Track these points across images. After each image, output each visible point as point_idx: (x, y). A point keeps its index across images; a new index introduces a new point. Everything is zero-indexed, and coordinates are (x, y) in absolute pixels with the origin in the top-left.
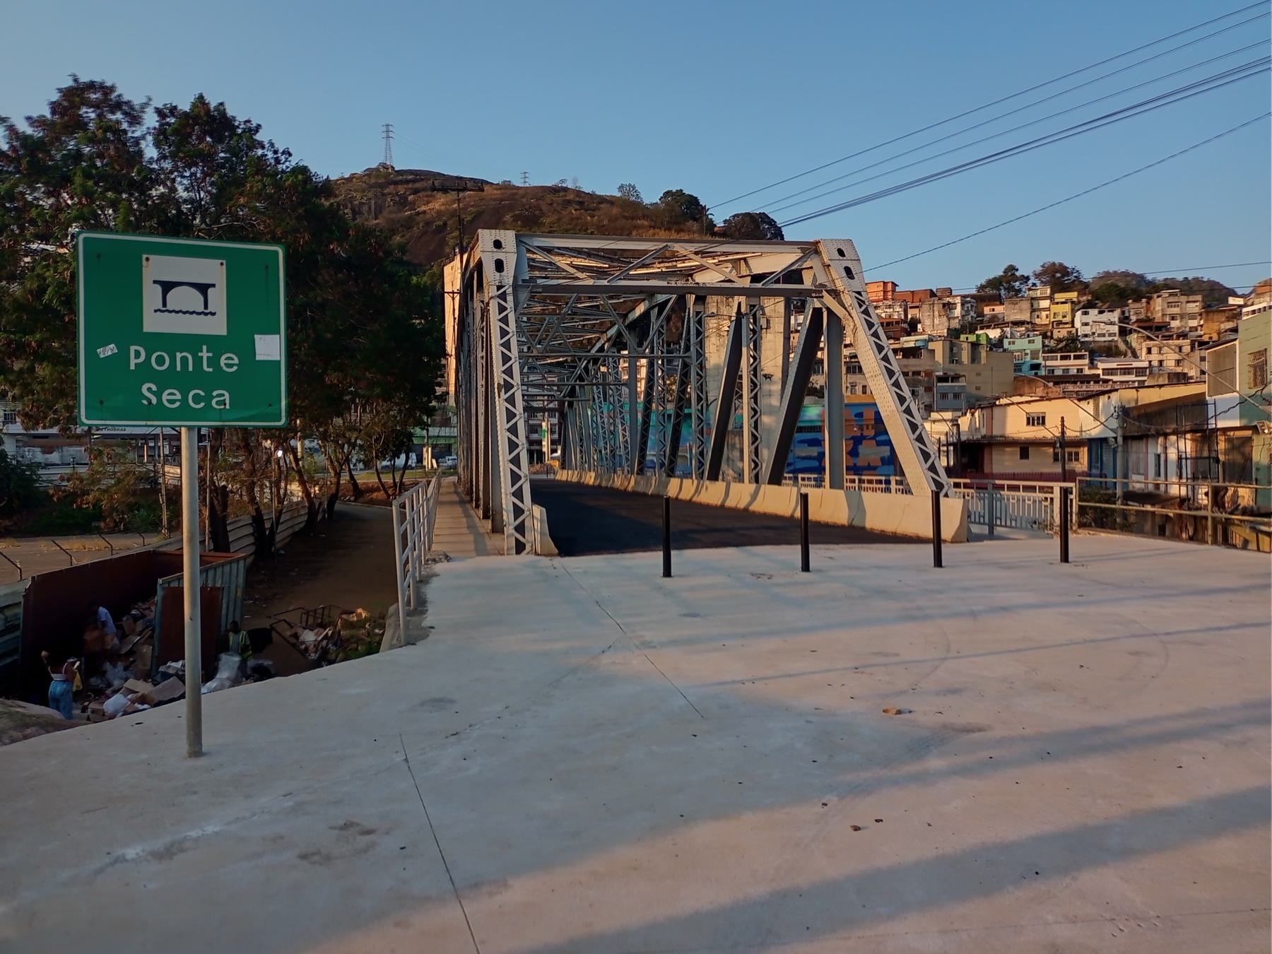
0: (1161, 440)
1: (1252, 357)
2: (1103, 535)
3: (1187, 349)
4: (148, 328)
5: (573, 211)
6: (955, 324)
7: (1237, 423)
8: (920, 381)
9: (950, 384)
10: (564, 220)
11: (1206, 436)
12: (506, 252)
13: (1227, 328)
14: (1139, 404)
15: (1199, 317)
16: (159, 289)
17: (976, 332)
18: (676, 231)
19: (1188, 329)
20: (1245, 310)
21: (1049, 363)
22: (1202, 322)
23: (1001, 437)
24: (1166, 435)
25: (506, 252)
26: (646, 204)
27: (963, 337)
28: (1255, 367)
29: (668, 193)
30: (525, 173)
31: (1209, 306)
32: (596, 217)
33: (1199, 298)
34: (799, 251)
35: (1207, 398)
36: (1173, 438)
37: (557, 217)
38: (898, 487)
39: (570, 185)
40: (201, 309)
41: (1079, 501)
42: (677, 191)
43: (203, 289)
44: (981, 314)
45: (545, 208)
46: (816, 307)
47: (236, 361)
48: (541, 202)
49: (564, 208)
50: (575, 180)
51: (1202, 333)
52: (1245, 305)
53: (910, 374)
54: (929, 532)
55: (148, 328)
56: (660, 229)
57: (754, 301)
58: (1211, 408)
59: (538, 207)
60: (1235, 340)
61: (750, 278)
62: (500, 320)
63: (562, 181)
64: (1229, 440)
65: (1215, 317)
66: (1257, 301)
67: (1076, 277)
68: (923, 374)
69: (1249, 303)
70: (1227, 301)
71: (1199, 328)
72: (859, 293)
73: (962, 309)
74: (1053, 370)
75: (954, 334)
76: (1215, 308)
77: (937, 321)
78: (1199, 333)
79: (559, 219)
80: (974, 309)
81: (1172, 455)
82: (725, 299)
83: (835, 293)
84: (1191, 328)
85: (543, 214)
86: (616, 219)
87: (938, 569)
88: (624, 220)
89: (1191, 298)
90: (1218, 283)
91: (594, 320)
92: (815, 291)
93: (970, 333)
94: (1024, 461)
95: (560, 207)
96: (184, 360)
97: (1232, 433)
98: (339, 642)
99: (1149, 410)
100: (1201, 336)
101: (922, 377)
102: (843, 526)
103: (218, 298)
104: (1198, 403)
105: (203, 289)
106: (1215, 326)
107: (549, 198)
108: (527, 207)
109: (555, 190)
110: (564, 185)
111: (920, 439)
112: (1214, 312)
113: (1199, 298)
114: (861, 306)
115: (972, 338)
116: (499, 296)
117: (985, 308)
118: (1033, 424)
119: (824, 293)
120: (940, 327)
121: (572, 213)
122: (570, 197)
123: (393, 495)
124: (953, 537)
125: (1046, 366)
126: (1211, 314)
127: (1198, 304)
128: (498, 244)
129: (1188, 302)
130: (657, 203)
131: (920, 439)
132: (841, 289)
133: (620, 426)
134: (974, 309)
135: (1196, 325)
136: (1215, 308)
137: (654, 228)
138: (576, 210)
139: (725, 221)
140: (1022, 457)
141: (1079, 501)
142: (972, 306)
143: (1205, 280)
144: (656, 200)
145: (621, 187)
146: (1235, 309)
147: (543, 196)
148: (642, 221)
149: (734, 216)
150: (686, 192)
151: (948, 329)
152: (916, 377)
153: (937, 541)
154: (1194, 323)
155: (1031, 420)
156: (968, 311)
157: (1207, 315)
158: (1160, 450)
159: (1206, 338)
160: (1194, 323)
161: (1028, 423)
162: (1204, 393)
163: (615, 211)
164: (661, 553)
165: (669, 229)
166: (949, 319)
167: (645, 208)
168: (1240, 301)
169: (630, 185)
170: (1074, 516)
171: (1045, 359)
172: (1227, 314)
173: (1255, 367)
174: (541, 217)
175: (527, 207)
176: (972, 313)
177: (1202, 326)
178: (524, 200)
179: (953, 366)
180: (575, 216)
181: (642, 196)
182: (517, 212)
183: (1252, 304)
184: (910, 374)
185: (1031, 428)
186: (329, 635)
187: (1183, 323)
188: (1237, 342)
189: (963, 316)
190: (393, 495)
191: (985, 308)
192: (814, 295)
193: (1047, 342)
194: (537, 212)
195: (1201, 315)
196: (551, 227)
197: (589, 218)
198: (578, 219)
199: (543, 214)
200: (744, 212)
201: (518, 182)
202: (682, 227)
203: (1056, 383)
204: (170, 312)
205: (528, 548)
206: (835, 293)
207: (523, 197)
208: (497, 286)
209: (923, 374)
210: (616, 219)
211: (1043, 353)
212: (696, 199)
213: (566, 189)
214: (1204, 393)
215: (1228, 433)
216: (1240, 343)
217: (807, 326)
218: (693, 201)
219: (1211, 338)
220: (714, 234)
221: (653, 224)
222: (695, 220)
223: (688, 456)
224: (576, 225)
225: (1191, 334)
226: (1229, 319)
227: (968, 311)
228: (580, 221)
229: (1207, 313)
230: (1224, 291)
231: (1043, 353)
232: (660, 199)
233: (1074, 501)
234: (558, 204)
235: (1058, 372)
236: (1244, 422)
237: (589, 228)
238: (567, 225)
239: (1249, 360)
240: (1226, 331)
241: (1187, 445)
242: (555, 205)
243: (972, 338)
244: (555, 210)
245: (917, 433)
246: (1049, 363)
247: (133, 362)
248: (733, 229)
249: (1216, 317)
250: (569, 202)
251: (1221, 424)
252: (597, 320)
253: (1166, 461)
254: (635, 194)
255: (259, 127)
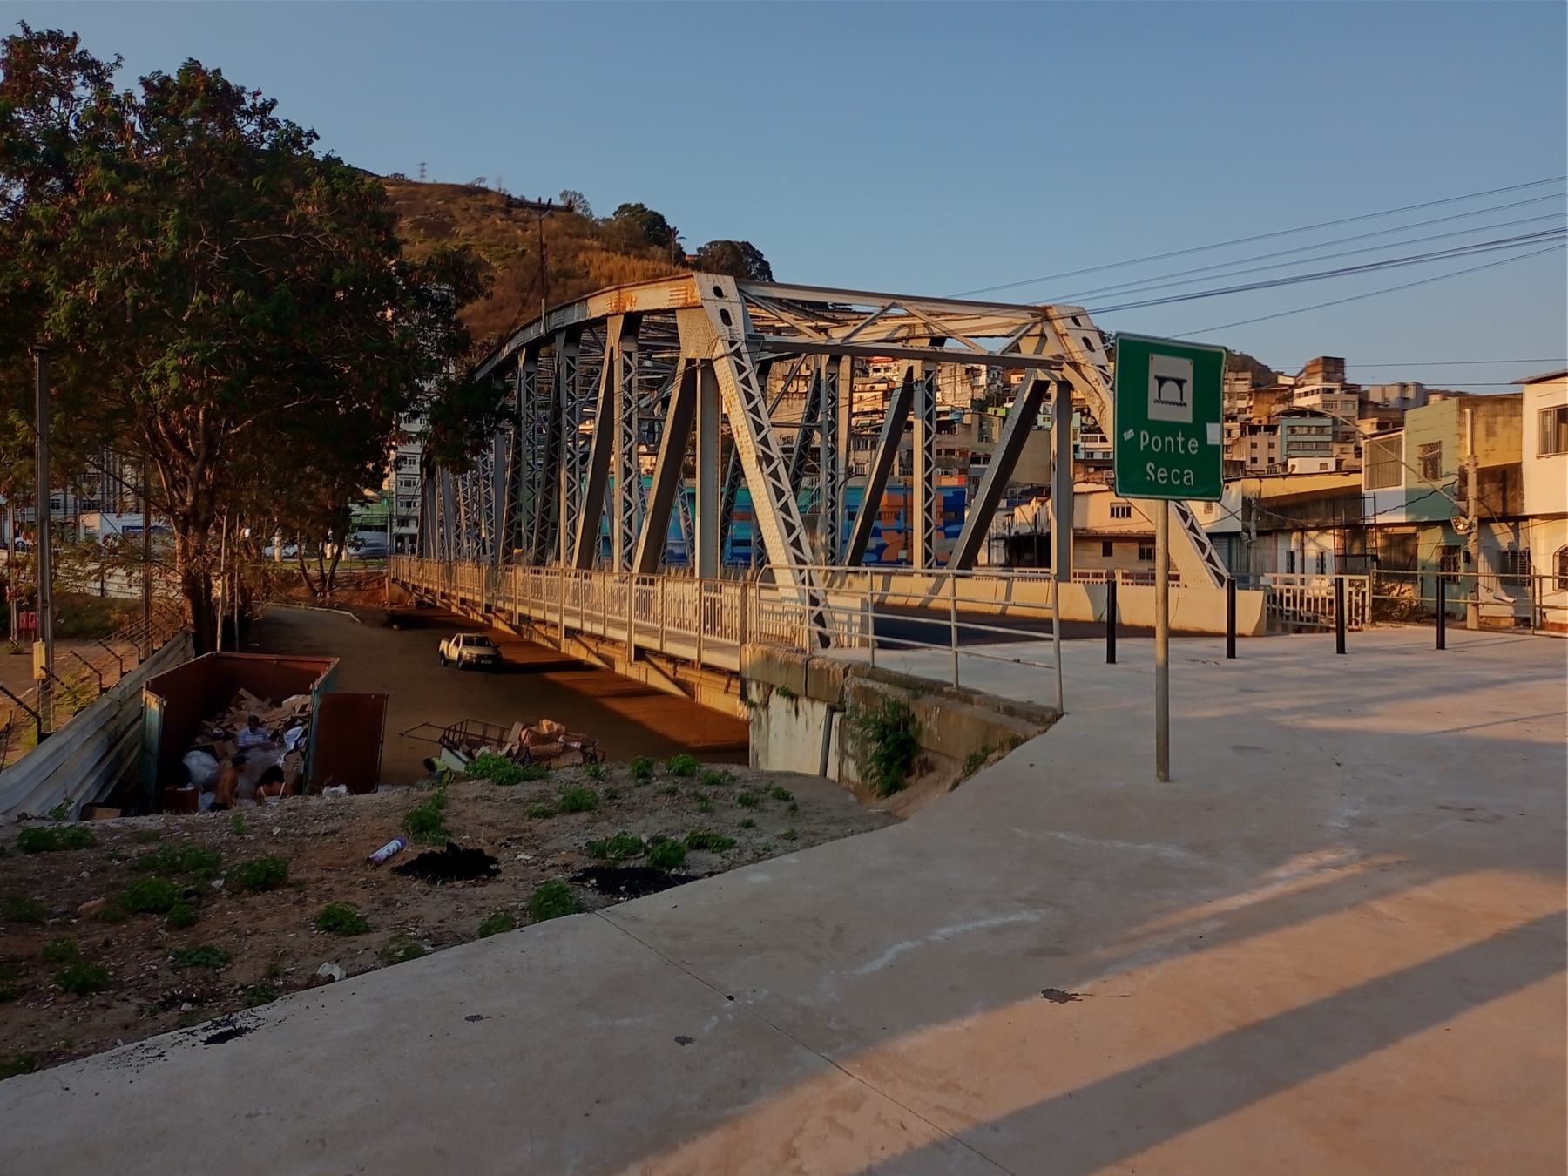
0: (1295, 535)
1: (1421, 449)
2: (1408, 627)
3: (1236, 433)
4: (1152, 415)
5: (498, 221)
6: (980, 394)
7: (1402, 519)
8: (954, 461)
9: (981, 466)
10: (484, 232)
11: (1356, 530)
12: (730, 302)
13: (1278, 411)
14: (1263, 496)
15: (1248, 398)
16: (1157, 382)
17: (1005, 405)
18: (635, 257)
19: (1236, 411)
20: (1297, 391)
21: (1089, 445)
22: (1251, 403)
23: (1083, 530)
24: (1303, 530)
25: (730, 302)
26: (597, 219)
27: (991, 410)
28: (1425, 460)
29: (624, 208)
30: (423, 164)
31: (1259, 385)
32: (529, 232)
33: (1248, 375)
34: (1029, 316)
35: (1364, 491)
36: (1313, 534)
37: (475, 227)
38: (1125, 581)
39: (491, 185)
40: (1178, 400)
41: (1374, 594)
42: (637, 205)
43: (1180, 383)
44: (1008, 384)
45: (457, 214)
46: (1040, 378)
47: (1197, 445)
48: (452, 206)
49: (485, 216)
50: (499, 180)
51: (1251, 415)
52: (1296, 386)
53: (943, 452)
54: (1224, 628)
55: (1152, 415)
56: (616, 253)
57: (930, 367)
58: (1369, 504)
59: (449, 213)
60: (1401, 430)
61: (929, 340)
62: (741, 382)
63: (481, 179)
64: (1388, 537)
65: (1265, 398)
66: (1308, 382)
67: (1112, 344)
68: (957, 453)
69: (1300, 383)
70: (1277, 381)
71: (1248, 410)
72: (1102, 367)
73: (988, 377)
74: (1092, 454)
75: (980, 406)
76: (1264, 388)
77: (958, 390)
78: (1249, 415)
79: (478, 230)
80: (1000, 377)
81: (1312, 551)
83: (1075, 366)
84: (1239, 409)
85: (455, 222)
86: (557, 236)
87: (1441, 651)
88: (567, 238)
89: (1241, 375)
90: (1251, 358)
91: (654, 374)
92: (1055, 363)
93: (998, 406)
94: (1106, 558)
95: (478, 215)
96: (1169, 442)
97: (1390, 529)
98: (527, 760)
99: (1284, 503)
100: (1250, 419)
101: (956, 457)
102: (1090, 623)
103: (1188, 388)
104: (1354, 495)
105: (1180, 383)
106: (1265, 408)
107: (463, 201)
109: (471, 191)
110: (483, 185)
111: (1192, 528)
112: (1263, 392)
113: (1248, 375)
114: (1107, 382)
115: (1001, 412)
116: (733, 354)
117: (1013, 377)
118: (1118, 516)
119: (1065, 366)
120: (963, 397)
121: (496, 224)
122: (492, 201)
123: (320, 591)
124: (1254, 631)
125: (1085, 449)
126: (1261, 394)
127: (1247, 382)
128: (718, 292)
129: (1237, 379)
130: (609, 220)
131: (1192, 528)
132: (1083, 361)
133: (681, 507)
134: (1000, 377)
135: (1245, 406)
136: (1264, 388)
137: (607, 251)
138: (502, 220)
139: (699, 250)
140: (1104, 555)
141: (1374, 594)
142: (999, 373)
143: (1238, 353)
144: (610, 215)
145: (564, 195)
146: (1286, 390)
147: (454, 199)
148: (591, 241)
149: (711, 244)
150: (649, 207)
151: (972, 400)
152: (949, 457)
153: (1231, 635)
154: (1242, 404)
155: (1114, 512)
156: (994, 379)
157: (1257, 396)
158: (1293, 547)
159: (1255, 422)
160: (1242, 404)
161: (1112, 515)
162: (1360, 486)
163: (554, 225)
164: (1105, 640)
165: (627, 254)
166: (973, 388)
167: (594, 224)
168: (1291, 382)
169: (575, 193)
170: (1367, 609)
171: (1084, 440)
172: (1278, 395)
173: (1425, 460)
174: (452, 225)
176: (999, 382)
177: (1251, 407)
179: (983, 444)
180: (499, 227)
181: (591, 208)
182: (418, 217)
183: (1303, 385)
184: (943, 452)
185: (1115, 520)
186: (515, 752)
187: (1231, 404)
188: (1403, 433)
189: (988, 385)
190: (320, 591)
191: (1013, 377)
192: (1053, 367)
193: (1084, 419)
194: (447, 219)
195: (1250, 394)
196: (466, 240)
197: (519, 231)
198: (504, 231)
199: (455, 222)
200: (724, 239)
201: (413, 176)
202: (644, 252)
203: (1097, 469)
204: (1162, 402)
205: (833, 641)
206: (1075, 366)
207: (426, 197)
208: (730, 342)
209: (957, 453)
210: (557, 236)
211: (1082, 432)
212: (661, 218)
213: (485, 191)
214: (1360, 486)
215: (1386, 529)
216: (1407, 434)
217: (1025, 399)
218: (658, 220)
219: (1260, 422)
220: (685, 265)
221: (605, 246)
222: (662, 244)
224: (503, 239)
225: (1242, 416)
226: (1280, 401)
227: (994, 379)
228: (506, 235)
229: (1257, 392)
230: (1258, 367)
231: (1082, 432)
232: (614, 214)
233: (1367, 595)
234: (476, 210)
235: (1098, 456)
236: (1410, 519)
237: (520, 244)
238: (490, 238)
239: (1418, 453)
240: (1278, 415)
241: (1329, 542)
242: (471, 211)
243: (1001, 412)
244: (472, 218)
245: (1189, 521)
246: (1089, 445)
247: (1142, 444)
248: (710, 260)
249: (1265, 397)
250: (491, 208)
251: (1381, 520)
252: (659, 374)
253: (1303, 559)
254: (583, 205)
255: (273, 103)
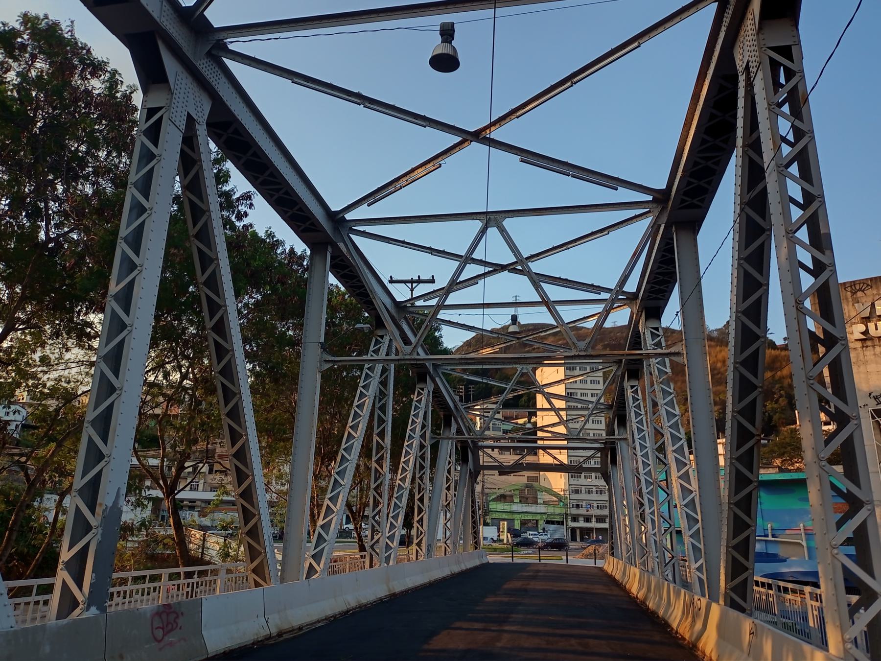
82: (849, 294)
108: (614, 338)
175: (614, 338)
178: (612, 334)
182: (606, 343)
223: (804, 543)
